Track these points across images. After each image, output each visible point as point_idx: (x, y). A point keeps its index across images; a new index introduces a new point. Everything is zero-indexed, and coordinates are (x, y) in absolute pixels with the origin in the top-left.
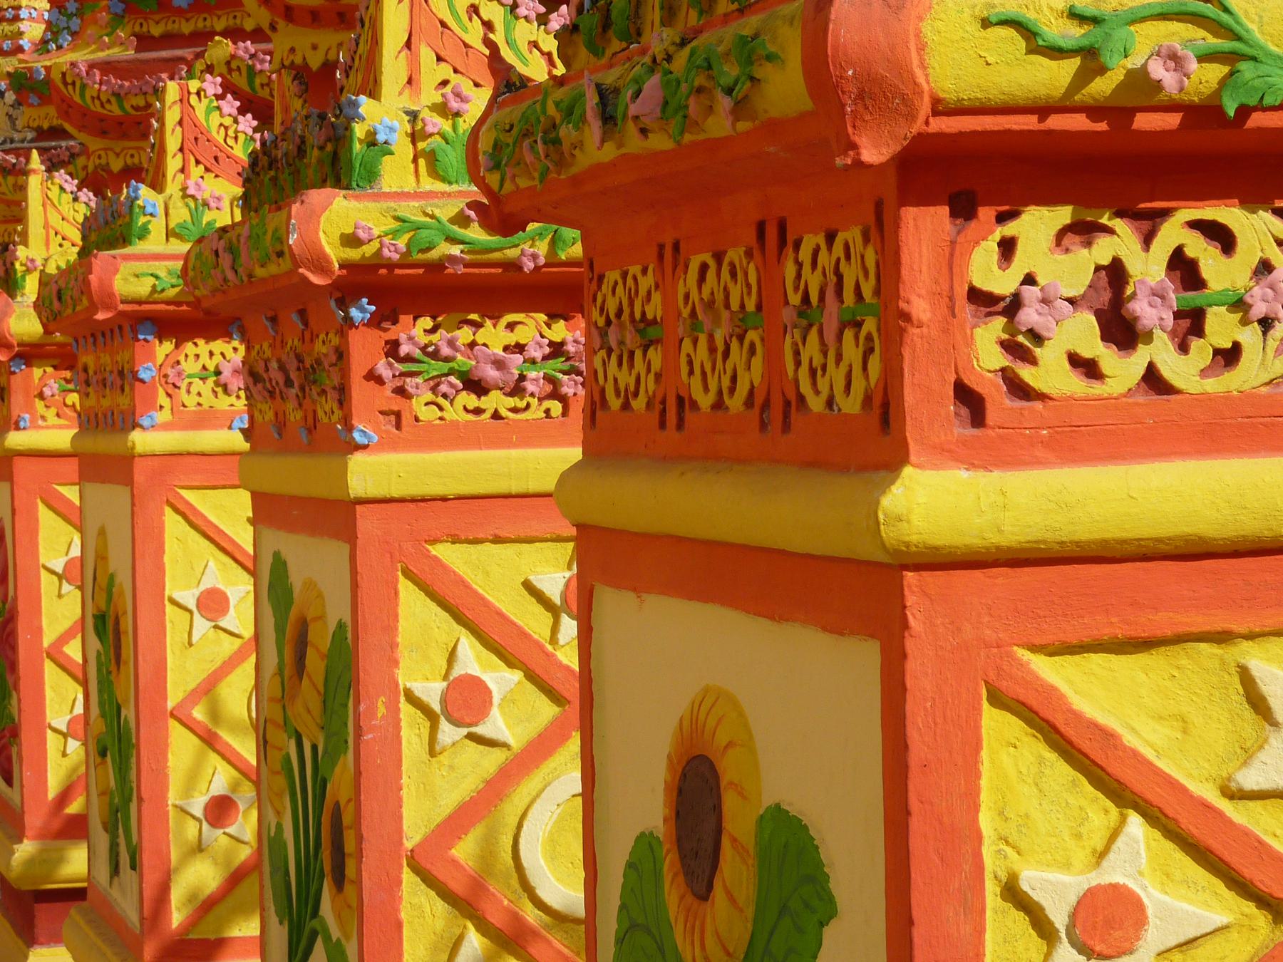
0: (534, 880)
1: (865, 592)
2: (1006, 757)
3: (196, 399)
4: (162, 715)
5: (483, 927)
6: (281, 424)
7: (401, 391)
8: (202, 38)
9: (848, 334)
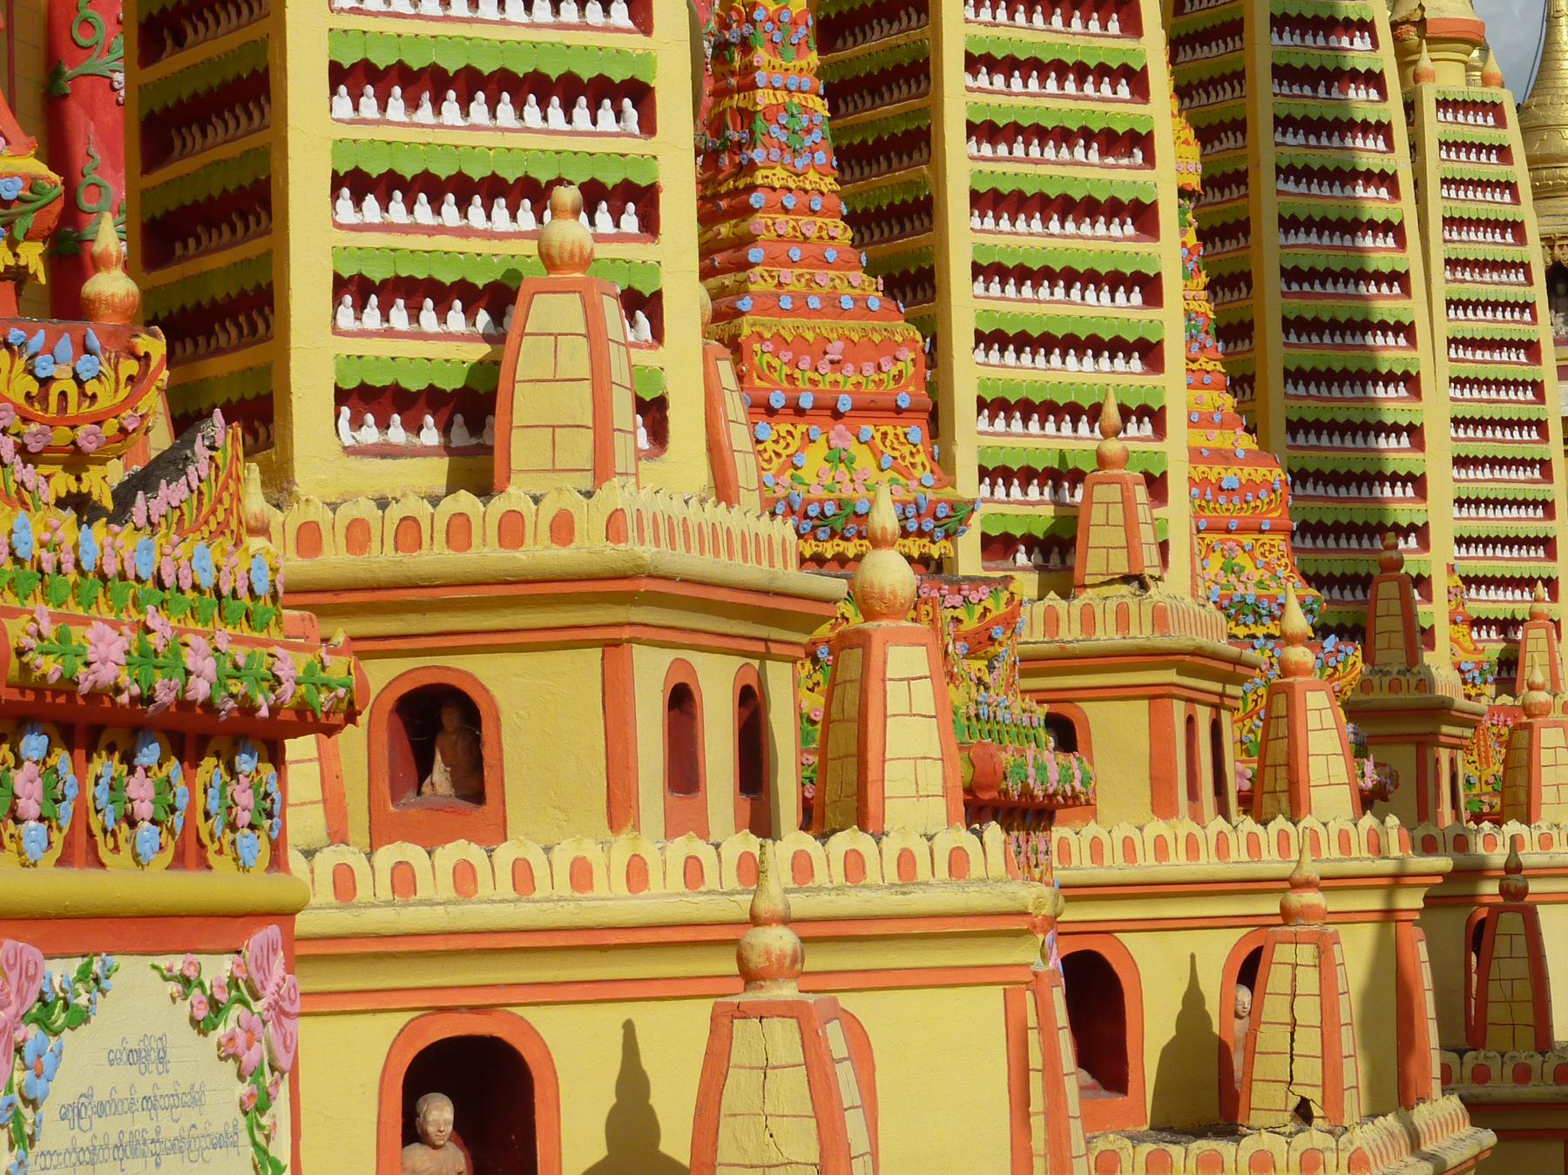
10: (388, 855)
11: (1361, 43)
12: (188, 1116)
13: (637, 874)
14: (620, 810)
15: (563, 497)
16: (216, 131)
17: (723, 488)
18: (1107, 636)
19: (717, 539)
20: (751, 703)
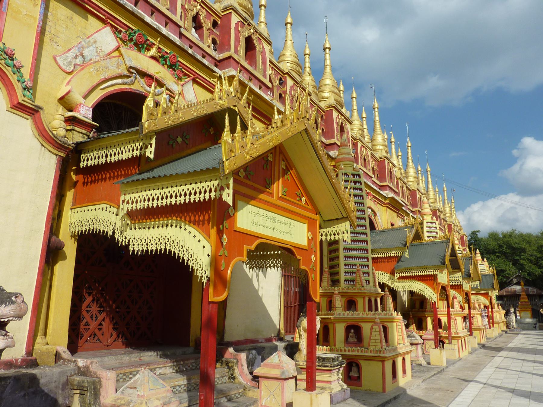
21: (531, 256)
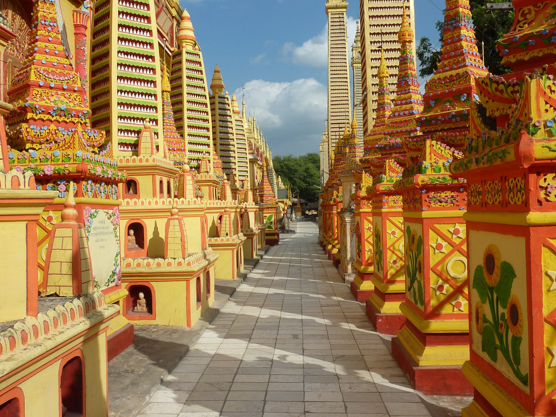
0: (449, 272)
1: (524, 231)
2: (545, 254)
3: (394, 205)
4: (386, 249)
5: (442, 279)
6: (409, 207)
7: (430, 203)
8: (391, 154)
9: (519, 193)
10: (126, 200)
11: (229, 112)
12: (108, 230)
13: (157, 203)
14: (154, 195)
15: (146, 157)
16: (102, 111)
17: (165, 157)
18: (204, 179)
19: (165, 163)
20: (169, 183)
21: (301, 175)
